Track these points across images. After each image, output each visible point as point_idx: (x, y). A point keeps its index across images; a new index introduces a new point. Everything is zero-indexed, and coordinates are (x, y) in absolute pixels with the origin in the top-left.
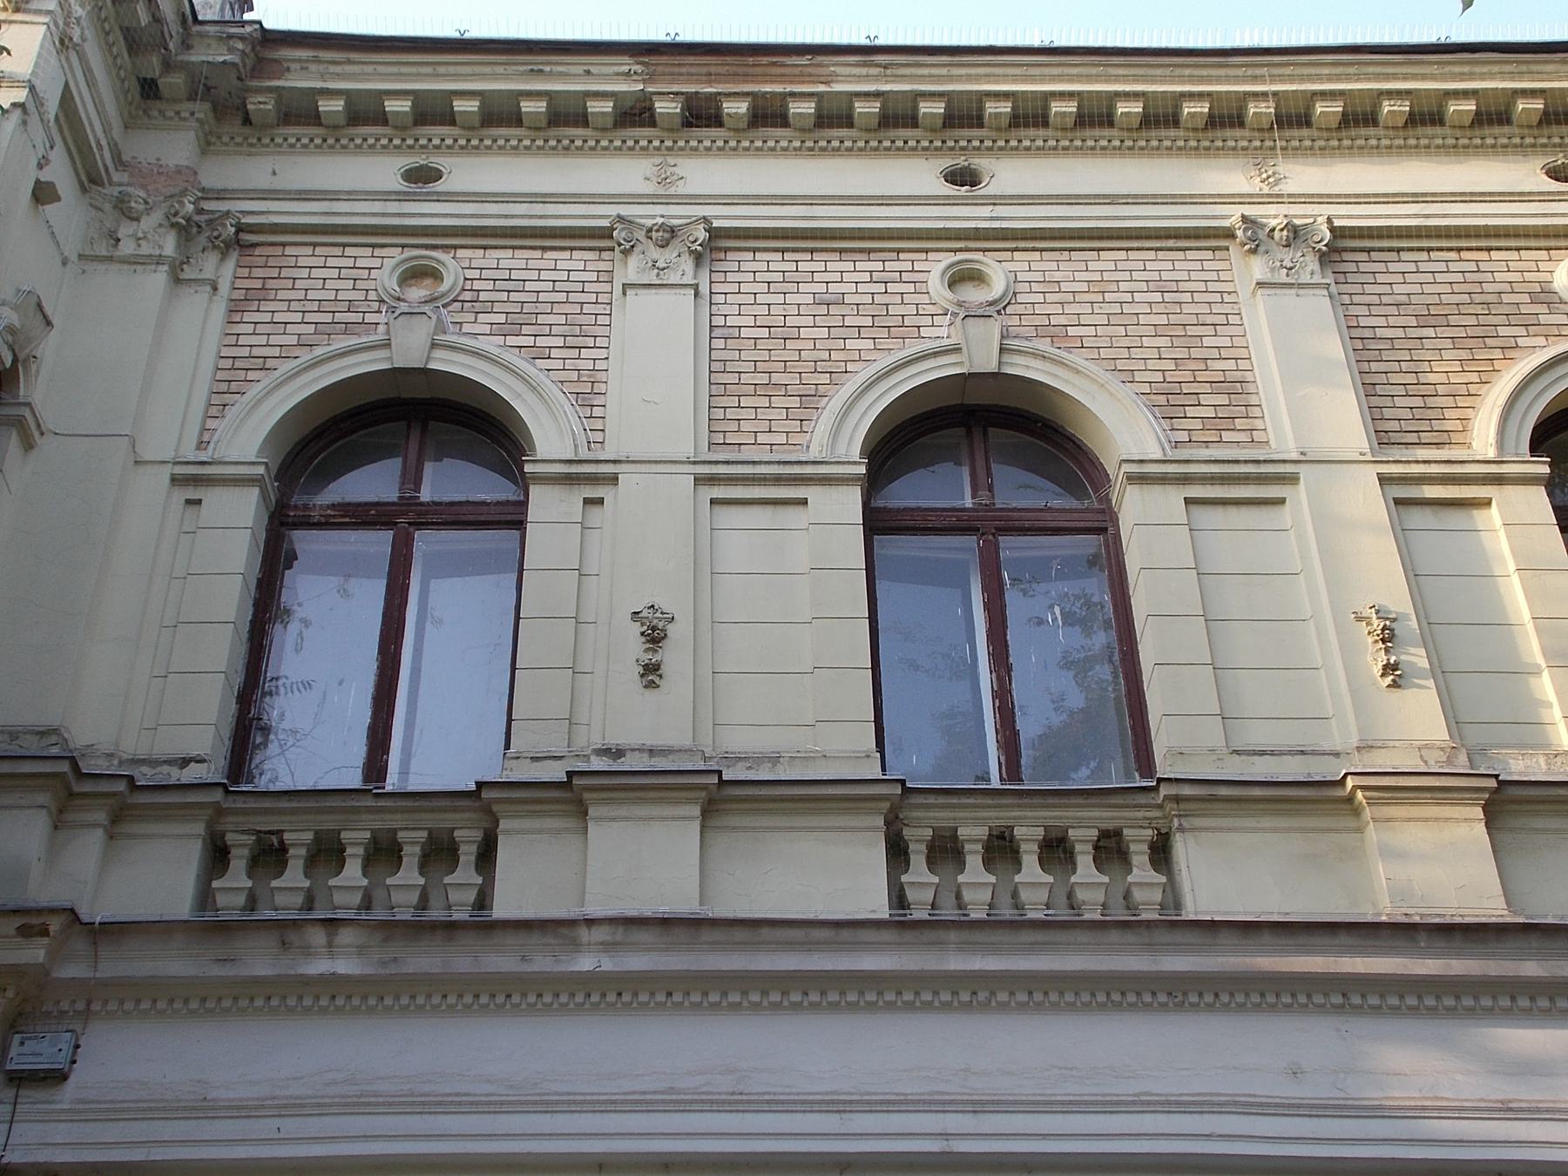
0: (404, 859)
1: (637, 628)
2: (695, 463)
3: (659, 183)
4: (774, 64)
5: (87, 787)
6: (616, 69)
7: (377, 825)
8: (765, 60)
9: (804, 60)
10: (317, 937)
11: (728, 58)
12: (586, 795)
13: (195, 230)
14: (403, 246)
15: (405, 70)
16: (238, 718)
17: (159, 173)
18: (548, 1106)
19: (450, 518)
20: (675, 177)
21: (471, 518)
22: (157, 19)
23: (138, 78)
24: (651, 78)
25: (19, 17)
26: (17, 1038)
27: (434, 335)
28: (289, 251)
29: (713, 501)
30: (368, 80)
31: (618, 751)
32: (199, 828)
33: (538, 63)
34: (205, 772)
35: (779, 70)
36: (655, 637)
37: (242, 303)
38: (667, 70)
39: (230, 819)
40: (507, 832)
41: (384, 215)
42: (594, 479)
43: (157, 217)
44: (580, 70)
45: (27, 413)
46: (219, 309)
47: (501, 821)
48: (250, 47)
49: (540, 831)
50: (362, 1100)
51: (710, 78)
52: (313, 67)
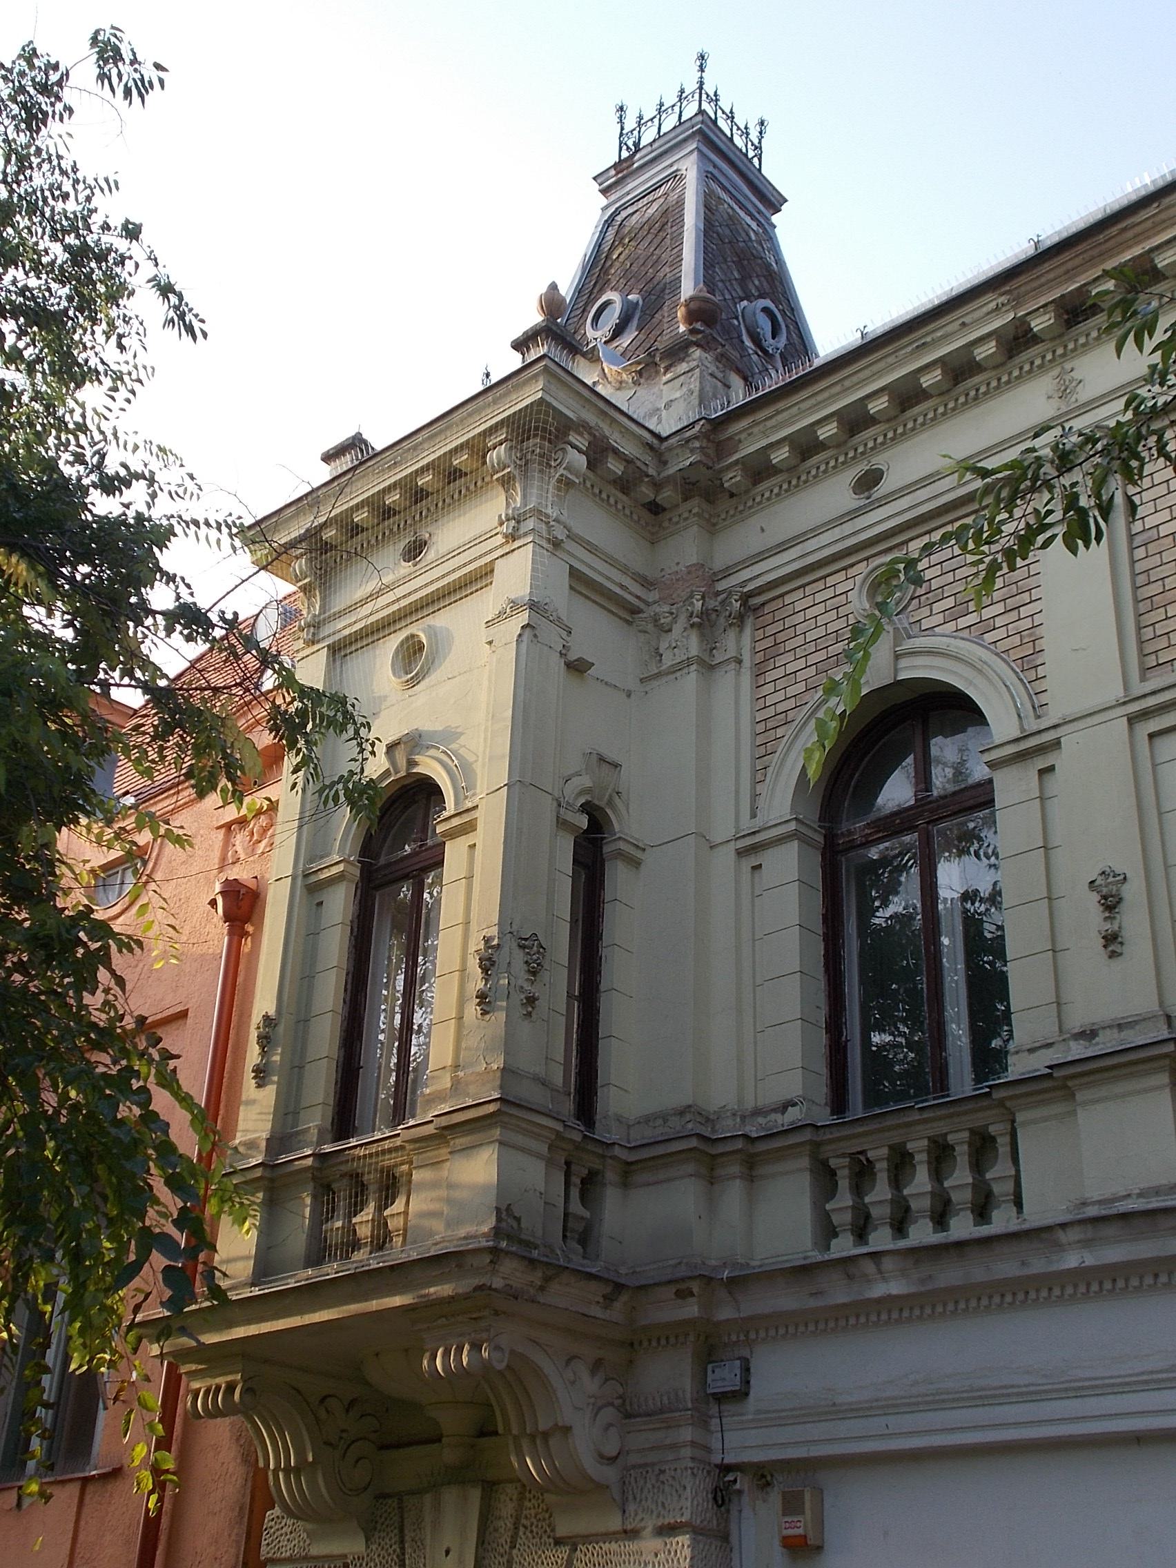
0: (958, 1158)
1: (1095, 897)
2: (1124, 703)
3: (1060, 397)
4: (1125, 229)
5: (721, 1148)
6: (985, 310)
7: (931, 1133)
8: (1114, 230)
9: (1152, 210)
10: (869, 1267)
11: (1080, 247)
12: (1070, 1084)
13: (714, 616)
14: (867, 559)
15: (820, 398)
16: (830, 1046)
17: (677, 580)
18: (1078, 1391)
19: (956, 808)
20: (1074, 384)
21: (972, 802)
22: (628, 461)
23: (643, 505)
24: (1017, 302)
25: (517, 544)
26: (710, 1367)
27: (896, 646)
28: (788, 600)
29: (1151, 736)
30: (798, 420)
31: (1092, 1031)
32: (805, 1162)
33: (920, 338)
34: (798, 1113)
35: (1130, 234)
36: (1111, 904)
37: (763, 665)
38: (1028, 287)
39: (829, 1148)
40: (1024, 1124)
41: (843, 538)
42: (1042, 750)
43: (682, 621)
44: (956, 325)
45: (622, 845)
46: (746, 679)
47: (1017, 1114)
48: (705, 441)
49: (1045, 1119)
50: (937, 1398)
51: (1070, 275)
52: (755, 430)
